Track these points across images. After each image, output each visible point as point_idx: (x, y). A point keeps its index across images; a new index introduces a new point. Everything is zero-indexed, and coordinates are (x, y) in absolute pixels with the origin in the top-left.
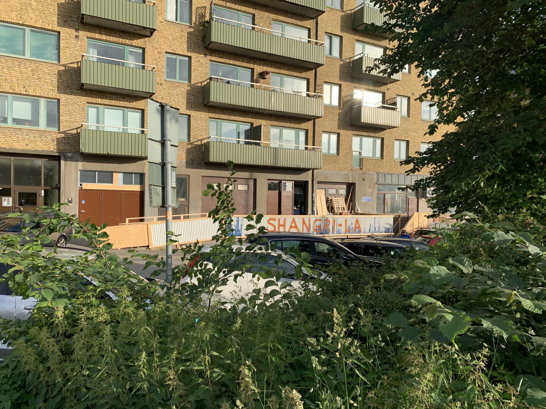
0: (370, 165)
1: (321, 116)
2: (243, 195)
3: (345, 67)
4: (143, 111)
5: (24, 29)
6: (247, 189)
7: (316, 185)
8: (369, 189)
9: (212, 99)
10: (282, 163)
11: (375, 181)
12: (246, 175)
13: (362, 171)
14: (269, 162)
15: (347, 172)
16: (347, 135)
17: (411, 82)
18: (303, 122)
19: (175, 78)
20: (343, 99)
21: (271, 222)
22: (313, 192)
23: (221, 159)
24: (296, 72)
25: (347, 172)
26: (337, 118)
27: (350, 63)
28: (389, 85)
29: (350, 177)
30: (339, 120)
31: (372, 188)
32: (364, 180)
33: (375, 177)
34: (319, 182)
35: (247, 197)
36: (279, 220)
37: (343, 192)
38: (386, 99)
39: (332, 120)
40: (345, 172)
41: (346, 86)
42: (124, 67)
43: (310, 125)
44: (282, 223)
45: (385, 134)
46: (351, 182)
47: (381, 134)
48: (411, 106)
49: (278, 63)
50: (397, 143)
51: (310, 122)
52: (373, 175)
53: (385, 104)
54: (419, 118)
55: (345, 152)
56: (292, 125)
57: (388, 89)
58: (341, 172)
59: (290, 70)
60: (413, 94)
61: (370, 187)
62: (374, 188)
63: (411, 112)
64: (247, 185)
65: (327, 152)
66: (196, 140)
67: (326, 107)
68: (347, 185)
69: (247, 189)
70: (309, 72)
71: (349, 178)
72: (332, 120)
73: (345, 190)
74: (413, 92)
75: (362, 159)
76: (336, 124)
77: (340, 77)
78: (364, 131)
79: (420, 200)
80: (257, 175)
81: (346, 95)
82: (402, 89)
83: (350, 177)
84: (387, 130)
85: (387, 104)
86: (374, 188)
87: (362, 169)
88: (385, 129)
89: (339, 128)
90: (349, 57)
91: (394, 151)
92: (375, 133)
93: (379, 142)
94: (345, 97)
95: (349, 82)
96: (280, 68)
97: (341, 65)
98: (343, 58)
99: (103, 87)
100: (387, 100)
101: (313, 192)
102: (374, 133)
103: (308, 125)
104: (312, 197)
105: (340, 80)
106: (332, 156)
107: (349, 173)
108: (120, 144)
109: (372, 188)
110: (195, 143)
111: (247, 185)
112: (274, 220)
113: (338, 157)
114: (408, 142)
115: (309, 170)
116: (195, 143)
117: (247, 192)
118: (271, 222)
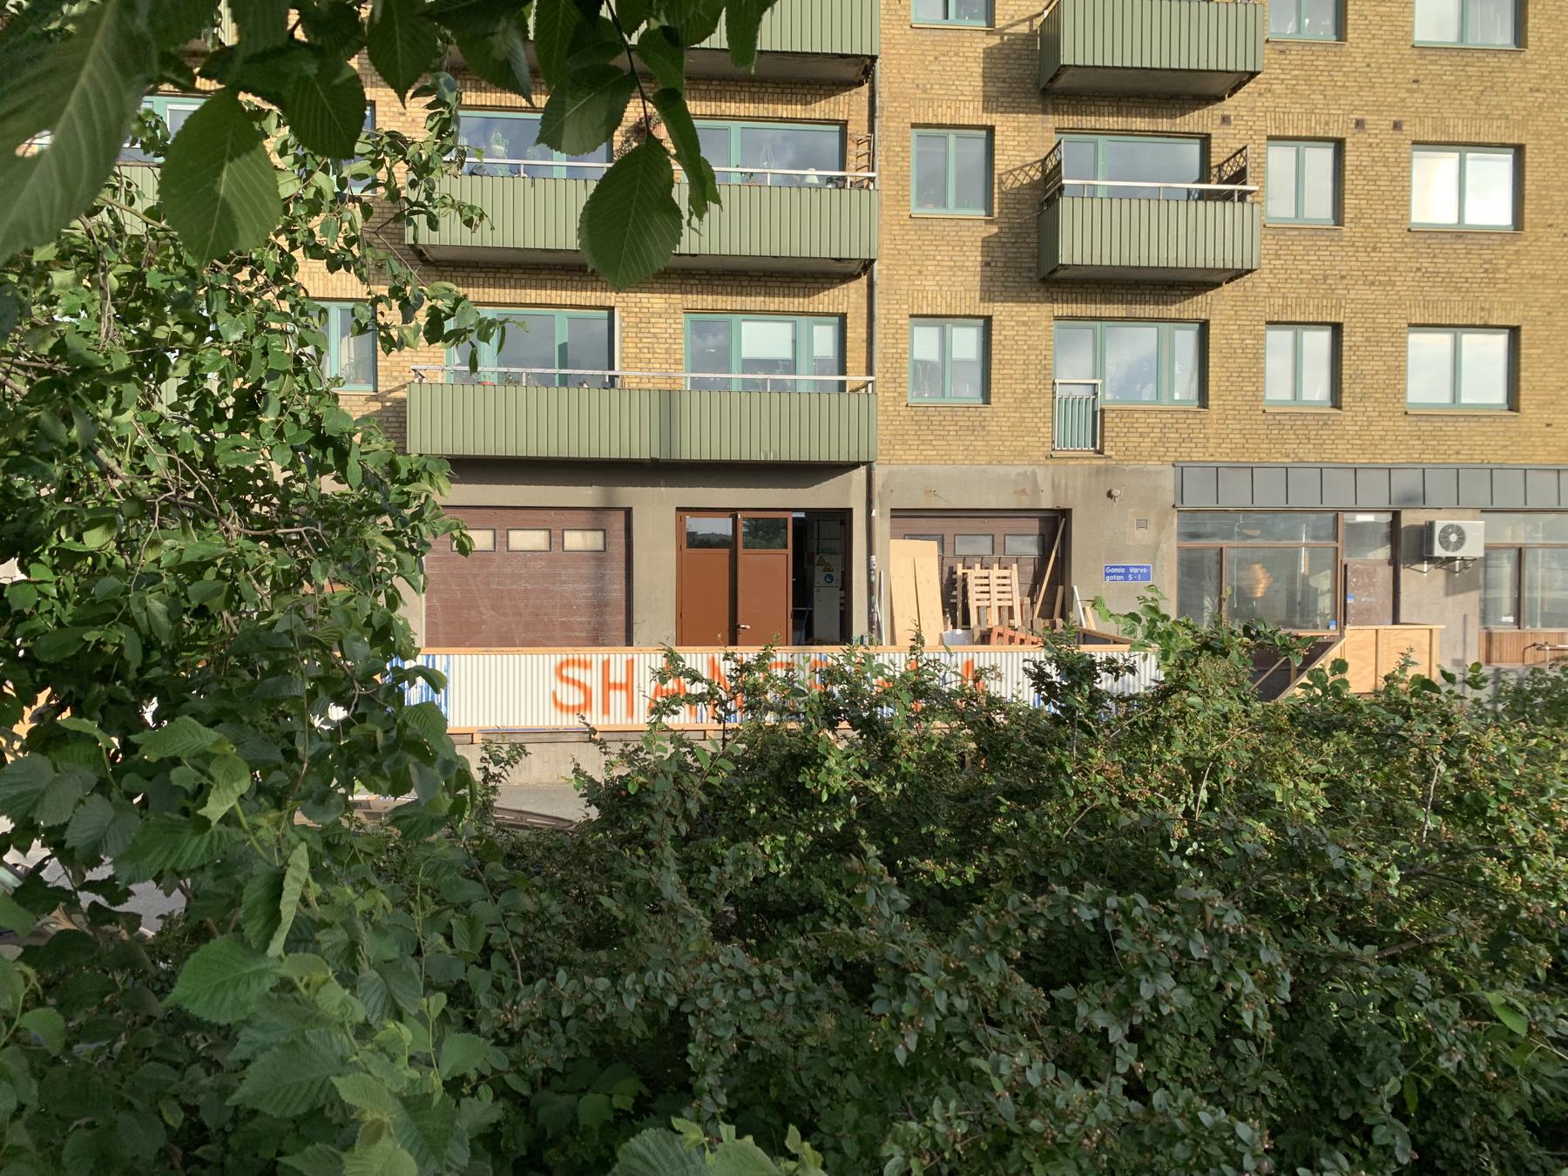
0: (1141, 435)
1: (1247, 266)
2: (586, 569)
3: (1007, 57)
4: (1204, 326)
5: (726, 129)
6: (600, 547)
7: (882, 525)
8: (1139, 534)
9: (1064, 258)
10: (692, 449)
11: (1169, 497)
12: (586, 495)
13: (1102, 462)
14: (642, 448)
15: (1030, 469)
16: (1025, 324)
17: (1345, 74)
18: (824, 289)
19: (945, 206)
20: (1001, 182)
21: (570, 672)
22: (870, 551)
23: (594, 445)
24: (789, 102)
25: (1030, 469)
26: (975, 258)
27: (1031, 36)
28: (1228, 102)
29: (1045, 486)
30: (988, 264)
31: (1152, 526)
32: (1110, 495)
33: (1168, 482)
34: (897, 513)
35: (600, 578)
36: (606, 665)
37: (1028, 547)
38: (1215, 161)
39: (951, 268)
40: (1021, 469)
41: (1019, 130)
42: (550, 183)
43: (853, 296)
44: (618, 675)
45: (1215, 305)
46: (1046, 503)
47: (1195, 307)
48: (1348, 174)
49: (709, 79)
50: (1280, 340)
51: (853, 285)
52: (1159, 473)
53: (1209, 182)
54: (1395, 221)
55: (1019, 388)
56: (774, 303)
57: (1225, 120)
58: (1000, 470)
59: (761, 100)
60: (1360, 124)
61: (1142, 524)
62: (1160, 528)
63: (1349, 201)
64: (600, 534)
65: (1288, 396)
66: (396, 384)
67: (1278, 231)
68: (1041, 519)
69: (600, 547)
70: (843, 98)
71: (1036, 490)
72: (951, 268)
73: (1034, 539)
74: (1357, 116)
75: (1103, 411)
76: (975, 282)
77: (987, 99)
78: (1108, 301)
79: (1405, 573)
80: (629, 495)
81: (1018, 164)
82: (1297, 109)
83: (1045, 486)
84: (1227, 287)
85: (1220, 182)
86: (1160, 528)
87: (1101, 452)
88: (1219, 285)
89: (988, 295)
90: (1028, 14)
91: (1262, 371)
92: (1165, 303)
93: (1186, 339)
94: (1011, 172)
95: (1029, 111)
96: (719, 97)
97: (989, 54)
98: (999, 24)
99: (544, 255)
100: (1220, 167)
101: (870, 551)
102: (1157, 303)
103: (849, 297)
104: (870, 571)
105: (985, 109)
106: (1476, 415)
107: (1037, 469)
108: (765, 420)
109: (1152, 526)
110: (393, 395)
111: (600, 534)
112: (586, 665)
113: (987, 412)
114: (1337, 328)
115: (856, 465)
116: (393, 395)
117: (599, 557)
118: (570, 672)
